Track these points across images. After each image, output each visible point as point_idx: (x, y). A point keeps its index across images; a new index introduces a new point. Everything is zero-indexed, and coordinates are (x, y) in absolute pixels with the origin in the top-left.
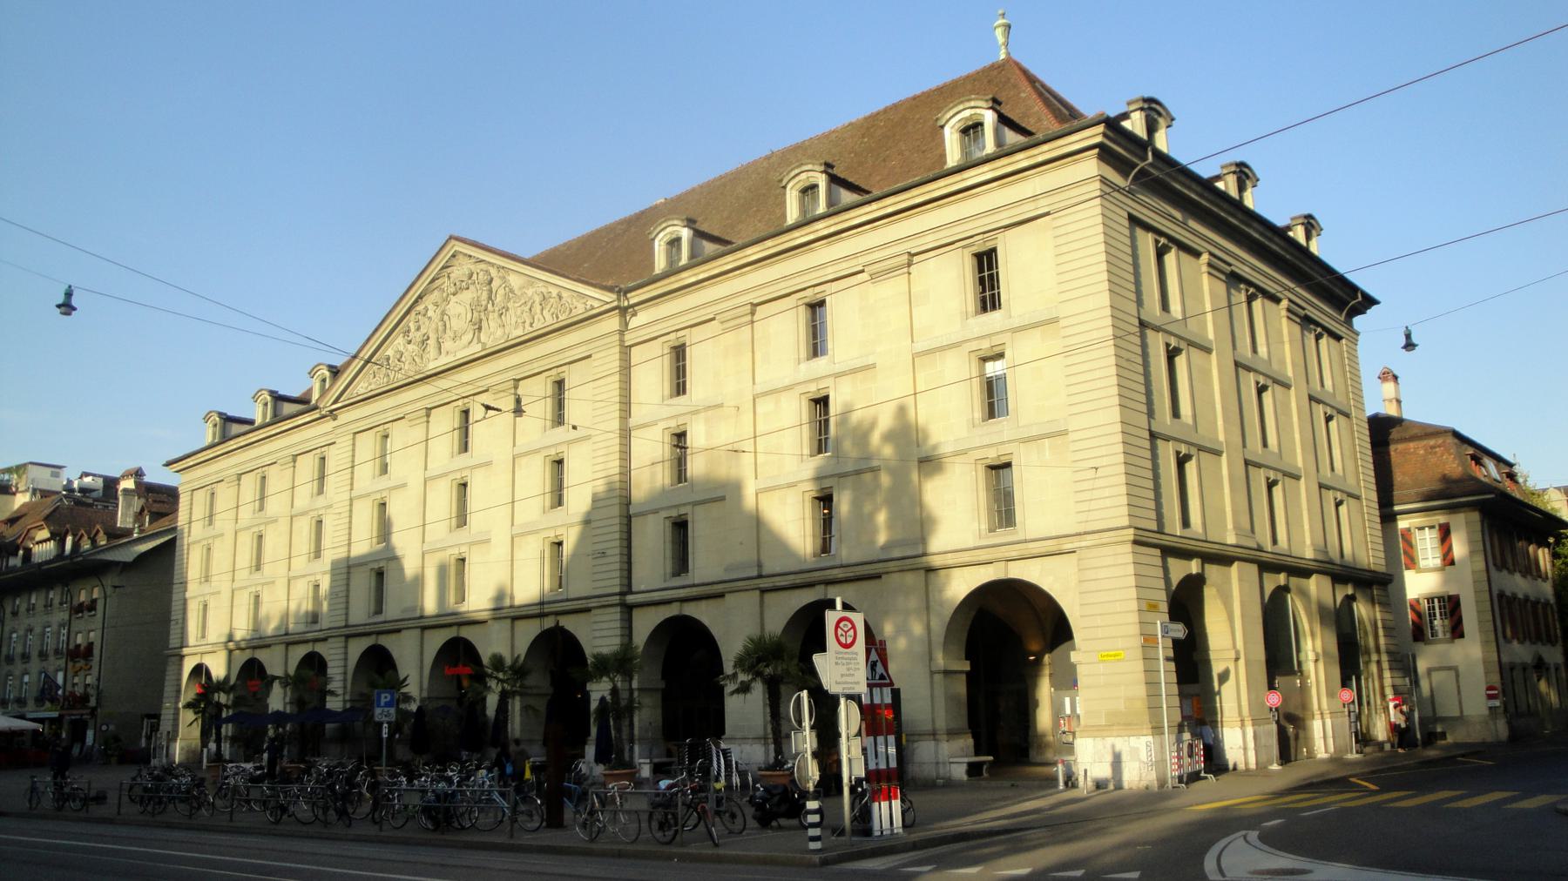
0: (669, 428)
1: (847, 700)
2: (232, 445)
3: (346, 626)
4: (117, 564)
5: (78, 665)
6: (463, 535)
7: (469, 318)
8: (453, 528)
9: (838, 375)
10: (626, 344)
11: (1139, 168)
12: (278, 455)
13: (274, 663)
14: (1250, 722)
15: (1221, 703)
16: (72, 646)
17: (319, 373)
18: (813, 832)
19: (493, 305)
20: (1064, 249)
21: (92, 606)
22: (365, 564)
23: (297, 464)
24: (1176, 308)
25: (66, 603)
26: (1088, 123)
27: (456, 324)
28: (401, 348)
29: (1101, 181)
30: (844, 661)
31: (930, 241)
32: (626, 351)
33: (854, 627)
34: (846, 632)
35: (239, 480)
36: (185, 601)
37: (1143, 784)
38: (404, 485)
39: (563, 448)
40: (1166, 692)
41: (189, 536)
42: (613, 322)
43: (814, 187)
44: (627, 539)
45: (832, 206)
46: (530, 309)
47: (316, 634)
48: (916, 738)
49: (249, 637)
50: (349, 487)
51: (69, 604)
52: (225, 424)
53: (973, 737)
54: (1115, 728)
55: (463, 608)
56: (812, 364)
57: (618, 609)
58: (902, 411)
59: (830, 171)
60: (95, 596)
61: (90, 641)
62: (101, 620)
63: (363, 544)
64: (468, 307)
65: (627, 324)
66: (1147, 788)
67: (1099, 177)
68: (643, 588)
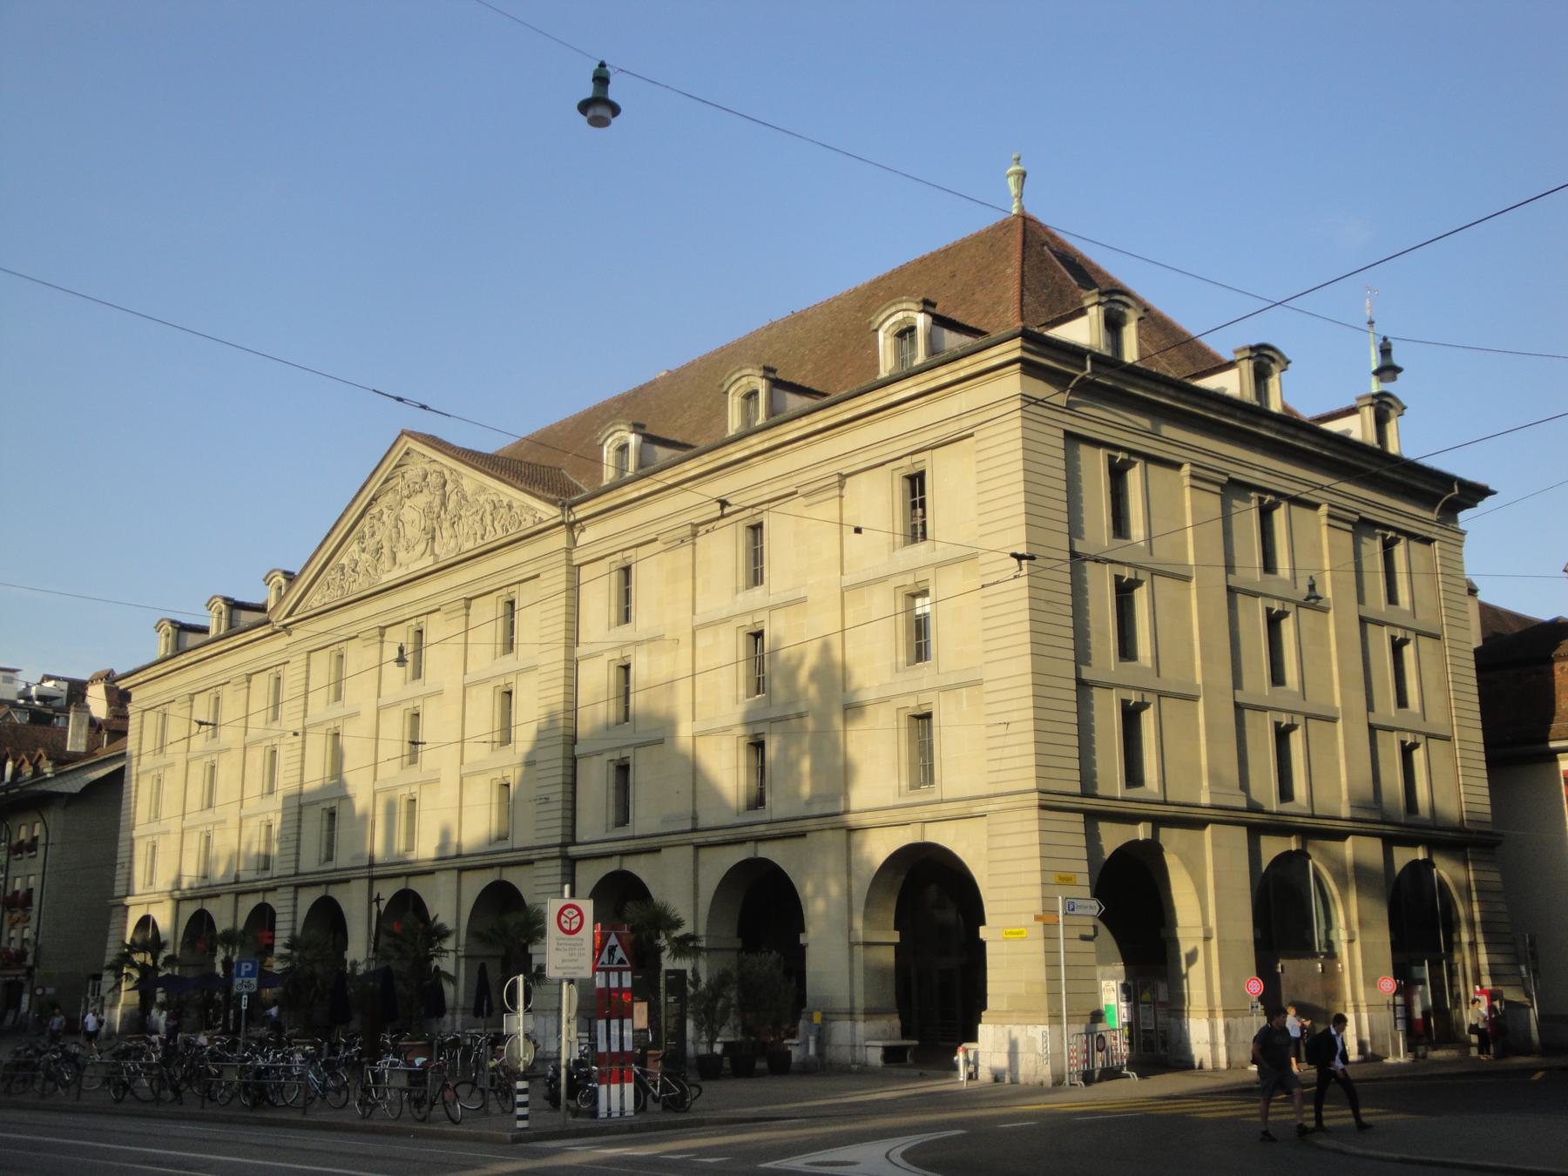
0: (614, 660)
1: (569, 984)
2: (183, 659)
3: (296, 874)
4: (60, 795)
5: (15, 916)
6: (414, 774)
7: (422, 527)
8: (405, 765)
9: (772, 608)
10: (575, 563)
11: (1077, 378)
12: (233, 673)
13: (224, 916)
14: (1222, 1013)
15: (1188, 990)
16: (9, 893)
17: (274, 580)
18: (520, 1111)
19: (446, 511)
20: (986, 476)
21: (32, 845)
22: (317, 803)
23: (252, 684)
24: (1137, 530)
25: (5, 841)
26: (1000, 338)
27: (412, 532)
28: (356, 557)
29: (1022, 399)
30: (567, 947)
31: (860, 461)
32: (574, 570)
33: (580, 914)
34: (571, 919)
35: (249, 681)
36: (132, 840)
37: (1038, 1079)
38: (357, 714)
39: (511, 679)
40: (1066, 976)
41: (138, 765)
42: (559, 539)
43: (755, 393)
44: (572, 784)
45: (774, 415)
46: (482, 519)
47: (265, 882)
48: (834, 1017)
49: (196, 885)
50: (302, 714)
51: (7, 844)
52: (178, 633)
53: (900, 1018)
54: (1015, 1014)
55: (412, 857)
56: (750, 594)
57: (559, 862)
58: (826, 648)
59: (931, 310)
60: (36, 833)
61: (30, 887)
62: (42, 861)
63: (316, 777)
64: (421, 511)
65: (575, 542)
66: (1042, 1084)
67: (1019, 396)
68: (586, 838)
